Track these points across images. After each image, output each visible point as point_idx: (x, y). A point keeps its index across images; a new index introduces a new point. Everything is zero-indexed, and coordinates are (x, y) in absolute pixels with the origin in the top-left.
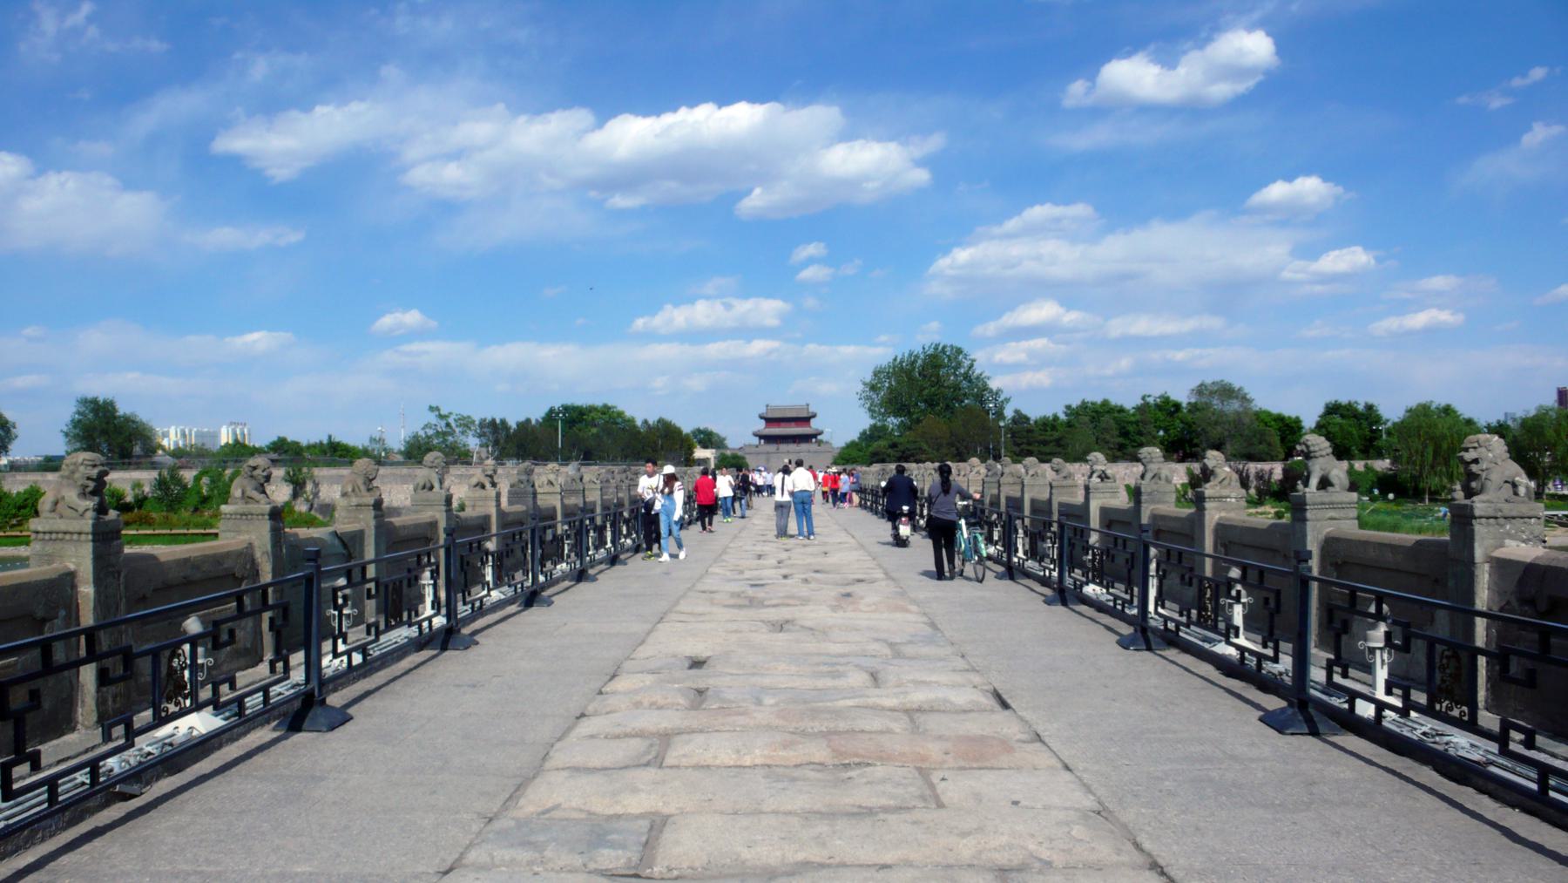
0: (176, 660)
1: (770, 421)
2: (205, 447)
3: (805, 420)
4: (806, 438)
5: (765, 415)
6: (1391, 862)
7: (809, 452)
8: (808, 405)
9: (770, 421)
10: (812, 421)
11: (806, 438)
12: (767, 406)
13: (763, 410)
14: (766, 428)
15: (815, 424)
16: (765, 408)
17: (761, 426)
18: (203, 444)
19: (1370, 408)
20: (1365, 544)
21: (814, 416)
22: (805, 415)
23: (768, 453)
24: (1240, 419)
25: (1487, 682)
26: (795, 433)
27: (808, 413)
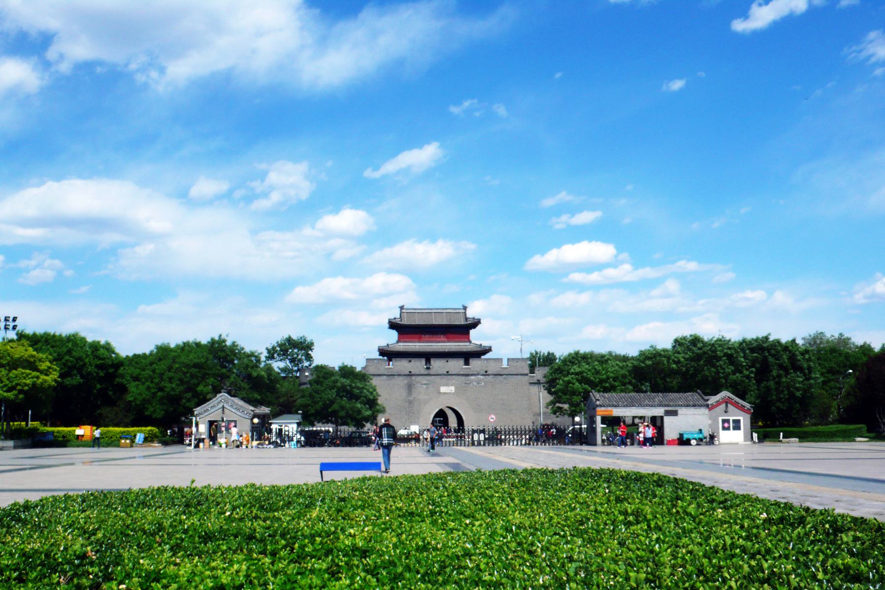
0: (147, 509)
1: (401, 328)
2: (812, 336)
3: (463, 329)
4: (467, 356)
5: (398, 321)
6: (158, 387)
7: (486, 374)
8: (465, 308)
9: (401, 328)
10: (472, 332)
11: (467, 356)
12: (402, 308)
13: (395, 314)
14: (398, 341)
15: (477, 337)
16: (398, 312)
17: (391, 338)
18: (841, 334)
19: (108, 344)
20: (744, 429)
21: (475, 324)
22: (462, 322)
23: (410, 375)
24: (715, 351)
25: (574, 445)
26: (429, 350)
27: (466, 319)
